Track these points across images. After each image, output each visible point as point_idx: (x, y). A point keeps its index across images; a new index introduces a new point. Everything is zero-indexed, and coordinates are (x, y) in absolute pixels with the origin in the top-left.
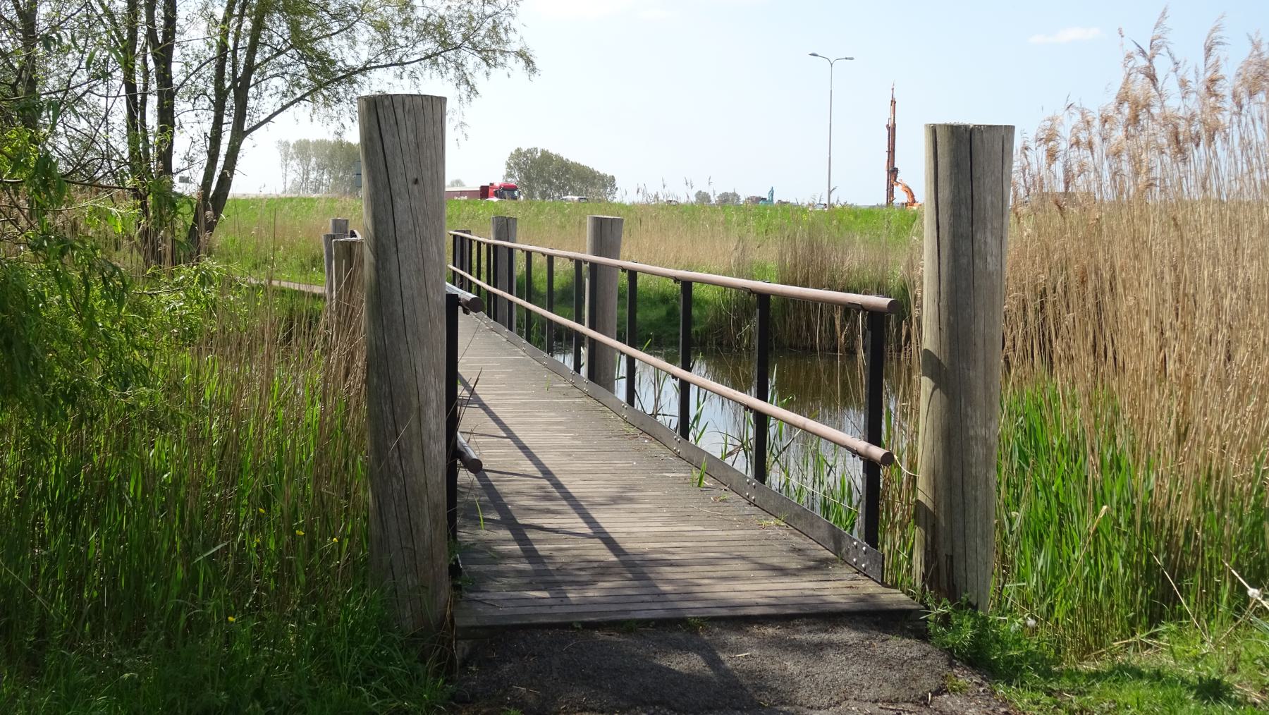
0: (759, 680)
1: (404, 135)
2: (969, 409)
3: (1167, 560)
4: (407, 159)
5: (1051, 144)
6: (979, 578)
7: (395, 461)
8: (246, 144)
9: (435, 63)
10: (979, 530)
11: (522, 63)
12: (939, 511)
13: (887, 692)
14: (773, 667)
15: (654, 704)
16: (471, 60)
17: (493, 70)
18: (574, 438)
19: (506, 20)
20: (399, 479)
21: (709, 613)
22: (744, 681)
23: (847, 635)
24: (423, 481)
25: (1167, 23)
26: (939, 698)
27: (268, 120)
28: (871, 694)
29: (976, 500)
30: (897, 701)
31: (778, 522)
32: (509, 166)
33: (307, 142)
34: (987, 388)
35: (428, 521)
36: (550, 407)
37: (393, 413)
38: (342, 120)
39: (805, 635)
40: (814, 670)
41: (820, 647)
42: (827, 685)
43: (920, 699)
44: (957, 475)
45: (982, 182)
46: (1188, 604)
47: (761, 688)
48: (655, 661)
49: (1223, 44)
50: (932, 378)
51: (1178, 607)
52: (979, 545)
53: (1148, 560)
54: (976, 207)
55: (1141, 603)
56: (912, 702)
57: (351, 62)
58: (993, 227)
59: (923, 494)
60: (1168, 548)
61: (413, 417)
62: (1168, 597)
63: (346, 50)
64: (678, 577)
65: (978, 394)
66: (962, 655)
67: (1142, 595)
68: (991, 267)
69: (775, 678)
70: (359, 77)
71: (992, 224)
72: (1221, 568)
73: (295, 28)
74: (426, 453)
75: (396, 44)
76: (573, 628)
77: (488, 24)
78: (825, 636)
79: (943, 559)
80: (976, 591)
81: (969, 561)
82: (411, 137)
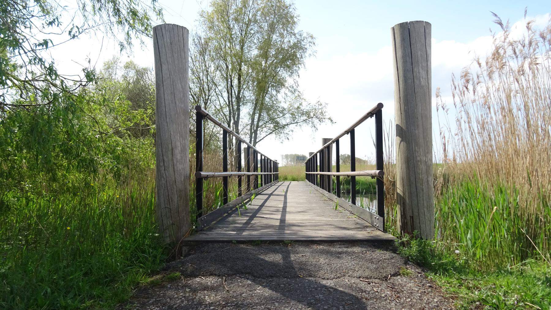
0: (303, 266)
1: (166, 39)
4: (167, 49)
6: (427, 227)
7: (163, 171)
9: (305, 122)
10: (425, 204)
11: (330, 121)
12: (406, 196)
13: (367, 273)
16: (316, 121)
19: (324, 110)
20: (164, 179)
23: (357, 249)
24: (174, 179)
26: (395, 278)
27: (263, 139)
28: (358, 274)
29: (423, 190)
30: (371, 278)
31: (355, 216)
34: (424, 138)
35: (176, 197)
37: (162, 151)
39: (337, 249)
43: (383, 278)
44: (413, 179)
46: (540, 250)
47: (301, 269)
51: (534, 251)
52: (426, 212)
53: (519, 231)
54: (413, 57)
55: (516, 250)
56: (379, 279)
57: (284, 123)
58: (422, 66)
59: (399, 189)
60: (528, 226)
65: (420, 141)
66: (414, 260)
67: (517, 246)
68: (423, 83)
69: (311, 265)
70: (286, 127)
71: (422, 64)
75: (296, 118)
76: (232, 243)
77: (320, 111)
78: (345, 249)
79: (409, 218)
80: (425, 234)
81: (421, 219)
82: (168, 40)
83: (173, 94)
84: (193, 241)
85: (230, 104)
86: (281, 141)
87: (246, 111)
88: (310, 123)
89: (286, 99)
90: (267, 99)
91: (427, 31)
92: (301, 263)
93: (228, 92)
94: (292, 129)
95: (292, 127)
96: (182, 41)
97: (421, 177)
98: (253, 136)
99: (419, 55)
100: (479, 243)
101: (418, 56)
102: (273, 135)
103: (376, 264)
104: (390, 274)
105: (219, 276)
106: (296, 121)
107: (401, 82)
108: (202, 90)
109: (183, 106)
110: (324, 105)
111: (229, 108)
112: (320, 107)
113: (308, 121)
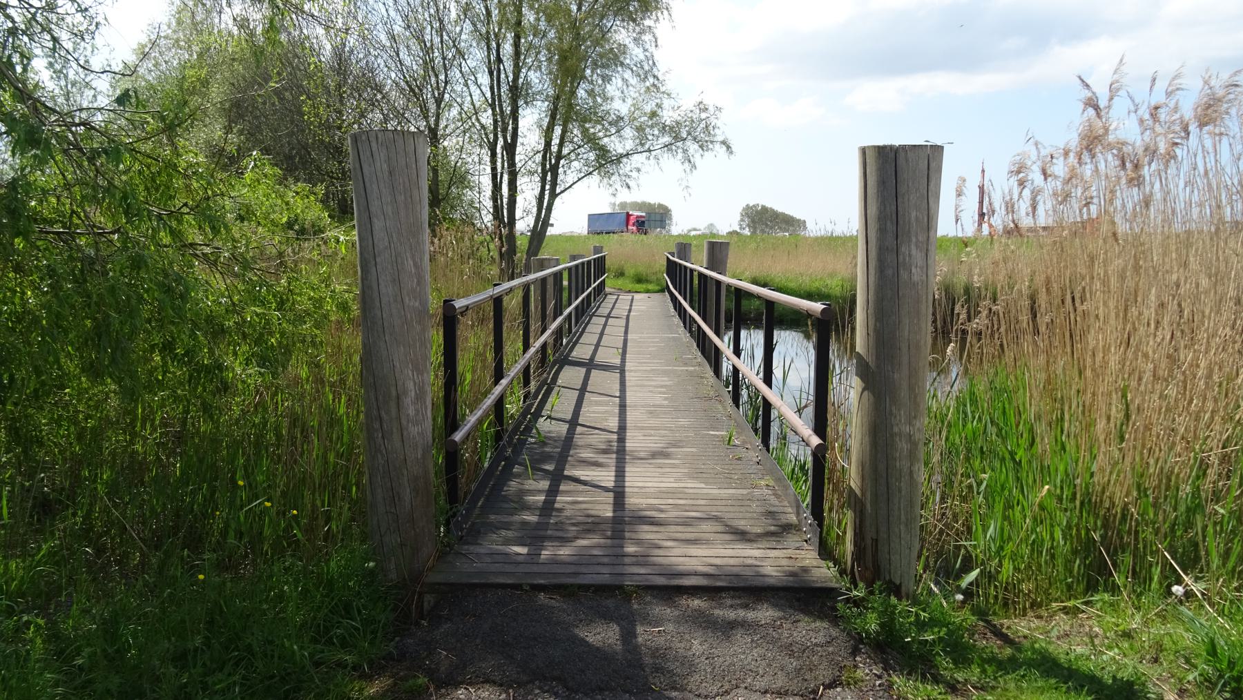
2: (893, 408)
3: (1103, 537)
4: (382, 185)
5: (1021, 175)
7: (380, 440)
8: (558, 201)
10: (903, 517)
13: (780, 682)
14: (679, 645)
15: (554, 679)
16: (693, 147)
17: (706, 153)
18: (666, 399)
19: (713, 121)
21: (647, 580)
22: (648, 660)
23: (765, 614)
25: (1124, 69)
27: (570, 187)
29: (900, 491)
32: (742, 215)
33: (626, 203)
34: (911, 388)
36: (665, 373)
37: (377, 399)
38: (616, 186)
40: (716, 652)
41: (732, 625)
42: (724, 670)
45: (906, 199)
47: (658, 669)
48: (577, 631)
49: (1182, 89)
50: (862, 379)
54: (901, 222)
57: (620, 151)
58: (917, 240)
60: (1105, 526)
61: (393, 404)
62: (1103, 569)
63: (617, 144)
64: (648, 537)
68: (915, 278)
69: (676, 659)
70: (625, 160)
71: (917, 238)
72: (1154, 548)
73: (585, 132)
74: (405, 434)
77: (703, 125)
78: (741, 613)
79: (869, 542)
81: (892, 545)
82: (385, 166)
83: (397, 281)
84: (445, 584)
85: (494, 103)
86: (611, 190)
87: (531, 120)
88: (680, 151)
89: (626, 91)
90: (581, 93)
91: (933, 165)
92: (655, 652)
93: (491, 73)
94: (639, 165)
95: (637, 160)
96: (414, 166)
97: (898, 465)
98: (549, 178)
99: (913, 219)
100: (1009, 548)
101: (910, 219)
102: (595, 177)
103: (798, 658)
104: (823, 684)
105: (501, 685)
106: (647, 146)
107: (872, 271)
108: (428, 65)
109: (417, 304)
110: (711, 109)
111: (494, 110)
112: (703, 115)
113: (674, 148)
